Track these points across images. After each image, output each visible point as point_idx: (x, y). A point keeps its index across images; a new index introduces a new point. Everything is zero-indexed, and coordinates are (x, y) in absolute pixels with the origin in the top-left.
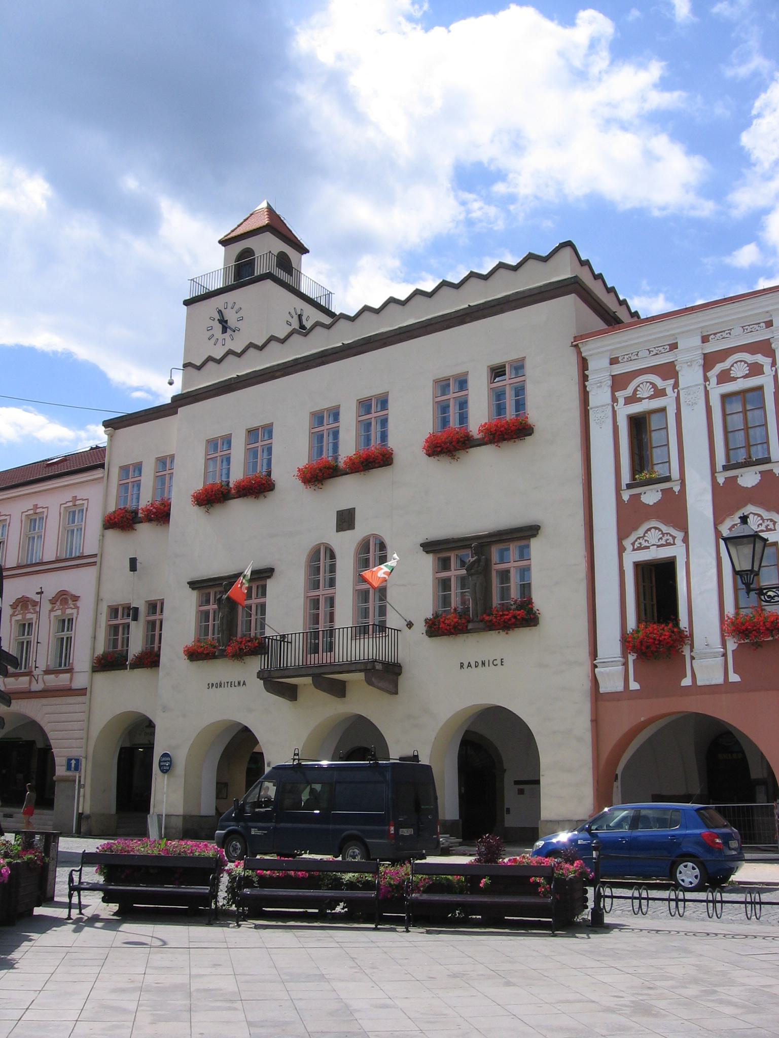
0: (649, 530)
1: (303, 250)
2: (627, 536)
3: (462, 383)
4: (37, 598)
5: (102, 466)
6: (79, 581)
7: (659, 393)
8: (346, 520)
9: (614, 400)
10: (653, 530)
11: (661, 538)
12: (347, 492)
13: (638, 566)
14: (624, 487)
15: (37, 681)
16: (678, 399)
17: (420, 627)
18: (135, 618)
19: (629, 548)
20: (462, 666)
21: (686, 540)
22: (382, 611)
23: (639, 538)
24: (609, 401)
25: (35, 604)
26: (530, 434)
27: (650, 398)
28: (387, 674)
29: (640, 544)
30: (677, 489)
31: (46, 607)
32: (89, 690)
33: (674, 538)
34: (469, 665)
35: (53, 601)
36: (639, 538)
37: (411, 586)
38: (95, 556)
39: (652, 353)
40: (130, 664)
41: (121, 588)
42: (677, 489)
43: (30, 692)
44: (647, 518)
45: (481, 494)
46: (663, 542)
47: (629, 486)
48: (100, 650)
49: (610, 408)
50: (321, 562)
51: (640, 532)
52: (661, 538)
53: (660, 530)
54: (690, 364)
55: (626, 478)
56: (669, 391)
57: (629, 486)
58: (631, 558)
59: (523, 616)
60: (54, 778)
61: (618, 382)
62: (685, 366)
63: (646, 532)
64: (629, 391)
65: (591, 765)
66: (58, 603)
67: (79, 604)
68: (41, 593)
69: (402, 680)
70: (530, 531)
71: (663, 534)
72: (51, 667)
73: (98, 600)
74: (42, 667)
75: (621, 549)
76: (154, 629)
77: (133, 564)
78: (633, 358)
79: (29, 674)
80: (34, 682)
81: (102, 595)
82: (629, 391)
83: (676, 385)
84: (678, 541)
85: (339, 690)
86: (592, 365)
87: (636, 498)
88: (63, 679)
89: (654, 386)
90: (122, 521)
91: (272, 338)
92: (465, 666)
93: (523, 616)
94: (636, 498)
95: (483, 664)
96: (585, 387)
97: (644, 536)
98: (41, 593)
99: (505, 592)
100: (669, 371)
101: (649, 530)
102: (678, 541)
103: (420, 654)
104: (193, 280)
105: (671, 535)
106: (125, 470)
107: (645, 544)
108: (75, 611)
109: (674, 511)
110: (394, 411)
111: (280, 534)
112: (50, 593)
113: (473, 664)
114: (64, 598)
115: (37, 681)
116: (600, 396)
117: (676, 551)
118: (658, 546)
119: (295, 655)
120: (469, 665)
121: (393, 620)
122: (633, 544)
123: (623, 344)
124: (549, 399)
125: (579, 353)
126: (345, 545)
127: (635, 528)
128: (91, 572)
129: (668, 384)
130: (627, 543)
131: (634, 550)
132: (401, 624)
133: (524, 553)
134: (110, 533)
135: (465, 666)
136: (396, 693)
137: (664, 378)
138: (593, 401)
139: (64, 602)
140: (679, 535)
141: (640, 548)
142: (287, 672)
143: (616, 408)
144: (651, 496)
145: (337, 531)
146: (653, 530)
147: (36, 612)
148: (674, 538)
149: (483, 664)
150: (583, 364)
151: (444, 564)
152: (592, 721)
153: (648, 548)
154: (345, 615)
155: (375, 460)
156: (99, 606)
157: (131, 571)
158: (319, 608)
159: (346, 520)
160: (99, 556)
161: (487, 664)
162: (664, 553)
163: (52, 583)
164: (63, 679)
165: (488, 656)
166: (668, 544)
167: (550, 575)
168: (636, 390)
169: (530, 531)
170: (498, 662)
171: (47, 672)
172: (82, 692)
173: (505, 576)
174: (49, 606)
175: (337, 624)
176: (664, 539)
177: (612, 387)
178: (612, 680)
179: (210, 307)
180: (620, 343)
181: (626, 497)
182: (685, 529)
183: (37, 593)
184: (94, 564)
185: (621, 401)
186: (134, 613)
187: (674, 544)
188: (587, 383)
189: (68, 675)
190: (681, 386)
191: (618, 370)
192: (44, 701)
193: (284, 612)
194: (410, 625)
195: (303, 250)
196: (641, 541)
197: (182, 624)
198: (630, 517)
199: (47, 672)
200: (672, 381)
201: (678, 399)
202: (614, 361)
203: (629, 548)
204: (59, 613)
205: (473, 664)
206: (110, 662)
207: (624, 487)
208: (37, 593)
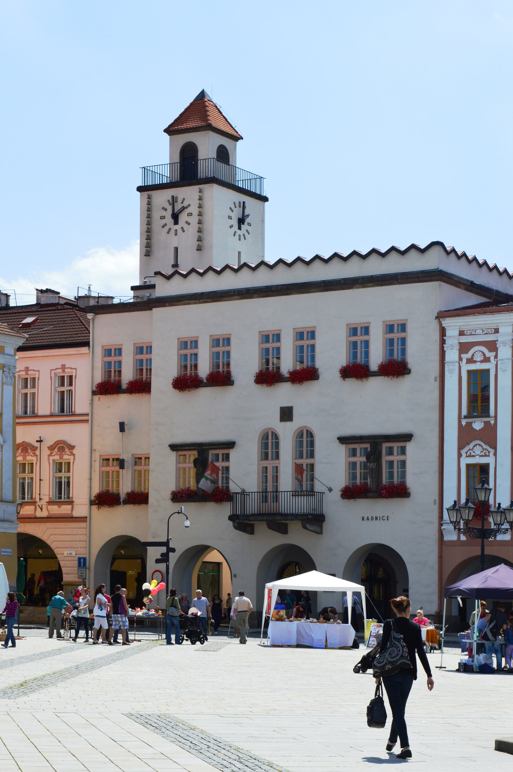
0: (476, 445)
1: (236, 138)
2: (463, 448)
3: (366, 330)
4: (37, 445)
5: (86, 344)
6: (75, 434)
7: (487, 360)
8: (286, 414)
9: (461, 359)
10: (478, 446)
11: (482, 451)
12: (285, 394)
13: (468, 466)
14: (463, 417)
15: (41, 509)
16: (497, 365)
17: (337, 494)
18: (122, 466)
19: (464, 455)
20: (363, 519)
21: (495, 454)
22: (312, 479)
23: (470, 450)
24: (457, 358)
25: (34, 449)
26: (409, 374)
27: (481, 362)
28: (315, 521)
29: (470, 453)
30: (492, 422)
31: (46, 452)
32: (88, 518)
33: (489, 452)
34: (368, 519)
35: (51, 448)
36: (470, 450)
37: (333, 468)
38: (87, 415)
39: (484, 333)
40: (123, 501)
41: (110, 443)
42: (492, 422)
43: (36, 518)
44: (475, 439)
45: (375, 408)
46: (483, 454)
47: (465, 417)
48: (96, 490)
49: (457, 364)
50: (269, 444)
51: (471, 446)
52: (482, 451)
53: (482, 446)
54: (504, 344)
55: (464, 412)
56: (492, 359)
57: (465, 417)
58: (465, 461)
59: (400, 491)
60: (62, 583)
61: (464, 348)
62: (501, 345)
63: (474, 447)
64: (469, 355)
65: (437, 583)
66: (56, 450)
67: (74, 452)
68: (40, 441)
69: (325, 525)
70: (408, 437)
71: (483, 449)
72: (54, 499)
73: (92, 450)
74: (46, 499)
75: (460, 455)
76: (141, 476)
77: (122, 427)
78: (473, 333)
79: (34, 503)
80: (38, 509)
81: (94, 447)
82: (469, 355)
83: (496, 357)
84: (492, 454)
85: (283, 529)
86: (448, 333)
87: (469, 424)
88: (65, 509)
89: (484, 354)
90: (108, 387)
91: (227, 267)
92: (365, 519)
93: (400, 491)
94: (469, 424)
95: (376, 518)
96: (443, 347)
97: (473, 449)
98: (40, 441)
99: (391, 475)
100: (492, 346)
101: (476, 445)
102: (492, 454)
103: (334, 506)
104: (144, 168)
105: (487, 450)
106: (108, 352)
107: (473, 454)
108: (72, 457)
109: (489, 437)
110: (320, 342)
111: (236, 415)
112: (49, 441)
113: (370, 519)
114: (62, 446)
115: (41, 509)
116: (452, 355)
117: (489, 460)
118: (480, 456)
119: (253, 506)
120: (368, 519)
121: (318, 487)
122: (466, 453)
123: (467, 324)
124: (419, 351)
125: (441, 324)
126: (286, 433)
127: (468, 444)
128: (84, 428)
129: (491, 355)
130: (463, 452)
131: (467, 456)
132: (323, 489)
133: (403, 451)
134: (96, 397)
135: (365, 519)
136: (321, 533)
137: (490, 351)
138: (448, 358)
139: (61, 450)
140: (492, 451)
141: (470, 456)
142: (248, 517)
143: (461, 365)
144: (478, 425)
145: (292, 407)
146: (478, 446)
147: (35, 455)
148: (489, 452)
149: (376, 518)
150: (443, 332)
151: (354, 453)
152: (439, 557)
153: (474, 456)
154: (287, 481)
155: (306, 375)
156: (93, 455)
157: (120, 431)
158: (269, 476)
159: (286, 414)
160: (90, 415)
161: (378, 518)
162: (483, 461)
163: (53, 433)
164: (65, 509)
165: (378, 513)
166: (486, 456)
167: (417, 465)
168: (473, 355)
169: (408, 437)
170: (385, 518)
171: (50, 503)
172: (83, 519)
173: (391, 463)
174: (49, 452)
175: (281, 488)
176: (484, 452)
177: (459, 350)
178: (451, 536)
179: (161, 198)
180: (465, 322)
181: (464, 423)
182: (495, 448)
183: (37, 441)
184: (87, 421)
185: (464, 361)
186: (121, 463)
187: (489, 456)
188: (445, 346)
189: (70, 507)
190: (499, 358)
191: (464, 339)
192: (49, 525)
193: (243, 472)
194: (330, 490)
195: (236, 138)
196: (471, 451)
197: (165, 475)
198: (466, 436)
199: (50, 503)
200: (494, 354)
201: (497, 365)
202: (462, 333)
203: (464, 455)
204: (57, 457)
205: (370, 519)
206: (106, 499)
207: (463, 417)
208: (37, 441)
